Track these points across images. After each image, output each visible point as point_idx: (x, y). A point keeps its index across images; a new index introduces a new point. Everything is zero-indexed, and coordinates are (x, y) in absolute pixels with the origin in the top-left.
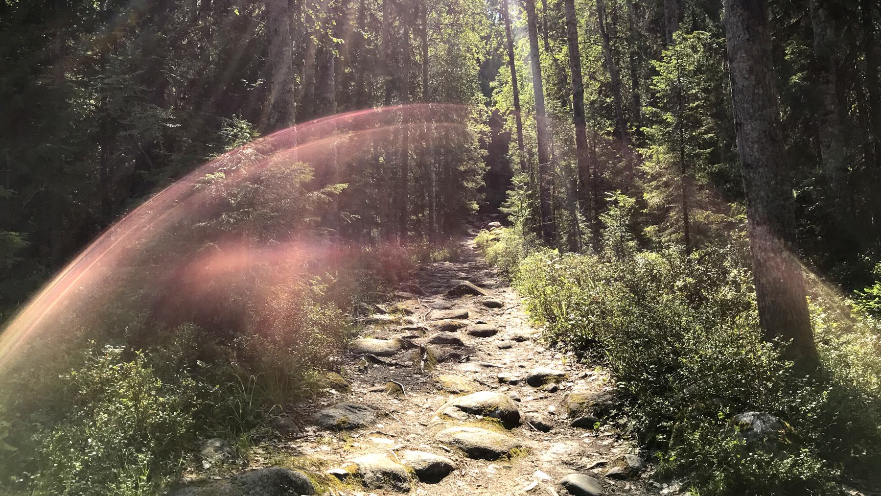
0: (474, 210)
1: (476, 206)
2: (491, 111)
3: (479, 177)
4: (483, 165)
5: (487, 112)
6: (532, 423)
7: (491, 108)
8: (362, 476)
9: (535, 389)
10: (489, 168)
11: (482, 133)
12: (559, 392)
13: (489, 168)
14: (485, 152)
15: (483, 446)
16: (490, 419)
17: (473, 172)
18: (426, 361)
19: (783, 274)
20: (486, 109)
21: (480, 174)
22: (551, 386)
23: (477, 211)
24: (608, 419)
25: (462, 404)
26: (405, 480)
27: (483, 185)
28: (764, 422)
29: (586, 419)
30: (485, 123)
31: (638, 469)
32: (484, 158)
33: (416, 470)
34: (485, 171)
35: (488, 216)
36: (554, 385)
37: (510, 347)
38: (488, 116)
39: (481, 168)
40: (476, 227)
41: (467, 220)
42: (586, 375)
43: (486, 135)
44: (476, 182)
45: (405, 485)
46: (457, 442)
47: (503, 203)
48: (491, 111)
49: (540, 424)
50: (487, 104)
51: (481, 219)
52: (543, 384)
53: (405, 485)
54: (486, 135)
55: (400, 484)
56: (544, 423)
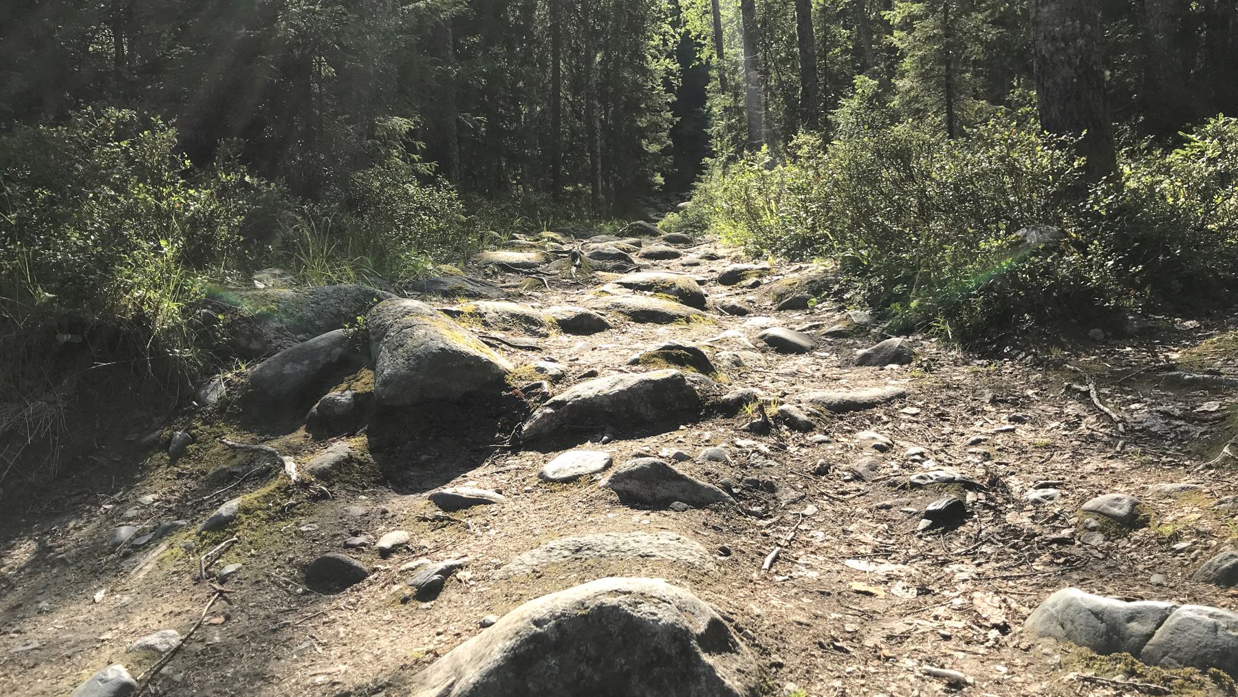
0: (657, 184)
1: (659, 179)
2: (680, 34)
3: (664, 134)
4: (669, 115)
5: (674, 37)
6: (722, 307)
7: (679, 30)
8: (481, 315)
9: (730, 287)
10: (678, 119)
11: (669, 72)
12: (761, 287)
13: (678, 119)
14: (672, 98)
15: (651, 308)
16: (664, 295)
17: (656, 127)
18: (579, 267)
19: (1076, 72)
20: (672, 32)
21: (665, 130)
22: (751, 281)
23: (662, 186)
24: (828, 295)
25: (623, 280)
26: (542, 325)
27: (669, 145)
28: (1041, 232)
29: (798, 298)
30: (669, 56)
31: (866, 324)
32: (673, 106)
33: (558, 321)
34: (672, 124)
35: (677, 195)
36: (755, 279)
37: (697, 264)
38: (675, 42)
39: (667, 120)
40: (660, 210)
41: (647, 201)
42: (801, 268)
43: (674, 75)
44: (661, 143)
45: (542, 330)
46: (617, 306)
47: (698, 176)
48: (680, 34)
49: (734, 307)
50: (674, 25)
51: (668, 200)
52: (740, 280)
53: (542, 330)
54: (674, 75)
55: (534, 328)
56: (738, 305)
